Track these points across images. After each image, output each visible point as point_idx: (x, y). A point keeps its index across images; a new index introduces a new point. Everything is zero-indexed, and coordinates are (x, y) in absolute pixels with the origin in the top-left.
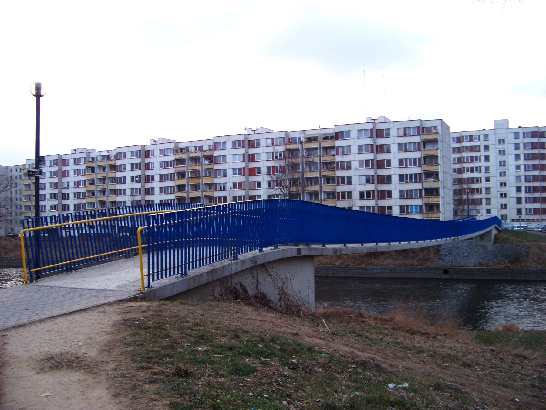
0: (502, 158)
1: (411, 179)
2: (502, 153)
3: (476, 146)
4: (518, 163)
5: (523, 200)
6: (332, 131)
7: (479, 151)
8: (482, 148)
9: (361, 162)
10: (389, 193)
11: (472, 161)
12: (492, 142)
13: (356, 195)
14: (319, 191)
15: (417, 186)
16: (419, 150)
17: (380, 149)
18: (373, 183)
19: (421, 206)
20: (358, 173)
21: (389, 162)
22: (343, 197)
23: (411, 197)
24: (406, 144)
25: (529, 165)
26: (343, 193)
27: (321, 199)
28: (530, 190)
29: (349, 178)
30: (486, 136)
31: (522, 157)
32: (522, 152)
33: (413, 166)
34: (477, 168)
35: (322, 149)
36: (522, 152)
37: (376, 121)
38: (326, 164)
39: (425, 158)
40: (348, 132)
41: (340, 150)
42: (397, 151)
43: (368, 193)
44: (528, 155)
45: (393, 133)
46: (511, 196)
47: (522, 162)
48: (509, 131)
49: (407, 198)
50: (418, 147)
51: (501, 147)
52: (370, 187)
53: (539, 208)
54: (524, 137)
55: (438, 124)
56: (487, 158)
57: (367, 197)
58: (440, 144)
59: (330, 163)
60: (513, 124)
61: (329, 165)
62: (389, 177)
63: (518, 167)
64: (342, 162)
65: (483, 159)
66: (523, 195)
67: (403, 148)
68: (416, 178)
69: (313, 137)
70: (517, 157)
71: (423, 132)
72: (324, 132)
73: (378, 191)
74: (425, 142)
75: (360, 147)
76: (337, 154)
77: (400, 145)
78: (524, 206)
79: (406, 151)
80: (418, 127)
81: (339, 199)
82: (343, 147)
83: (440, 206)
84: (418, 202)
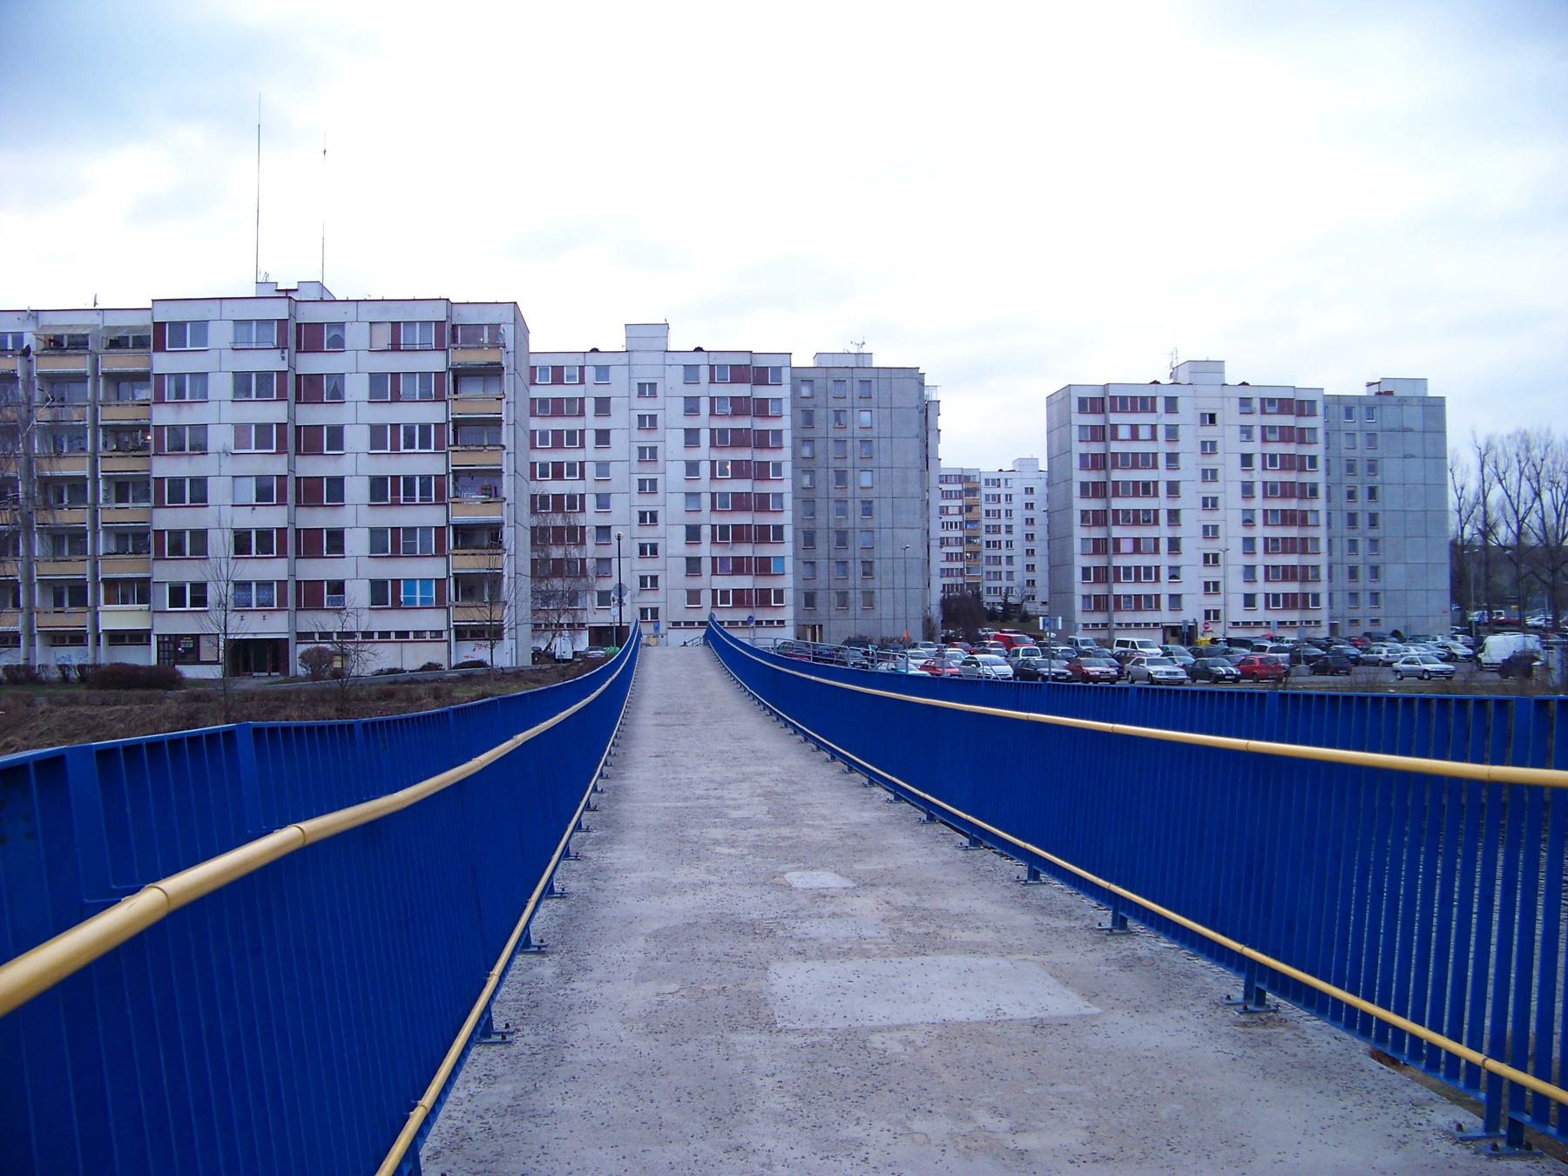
0: (645, 438)
1: (409, 491)
2: (648, 422)
3: (571, 400)
4: (694, 455)
5: (706, 566)
6: (145, 321)
7: (582, 414)
8: (590, 406)
9: (241, 430)
10: (336, 540)
11: (558, 445)
12: (619, 388)
13: (220, 543)
14: (88, 526)
15: (431, 516)
16: (440, 398)
17: (310, 389)
18: (282, 501)
19: (440, 582)
20: (231, 467)
21: (337, 436)
22: (177, 549)
23: (410, 553)
24: (395, 375)
25: (723, 464)
26: (177, 536)
27: (95, 555)
28: (724, 536)
29: (200, 484)
30: (603, 372)
31: (705, 437)
32: (703, 422)
33: (417, 450)
34: (571, 466)
35: (101, 380)
36: (703, 422)
37: (295, 296)
38: (114, 431)
39: (457, 424)
40: (201, 326)
41: (169, 387)
42: (367, 399)
43: (265, 535)
44: (723, 432)
45: (356, 336)
46: (670, 551)
47: (703, 452)
48: (669, 359)
49: (396, 554)
50: (437, 388)
51: (646, 406)
52: (273, 517)
53: (749, 590)
54: (712, 381)
55: (506, 316)
56: (603, 437)
57: (260, 549)
58: (507, 379)
59: (131, 429)
60: (680, 341)
61: (129, 438)
62: (337, 484)
63: (692, 468)
64: (176, 430)
65: (590, 438)
66: (705, 550)
67: (385, 388)
68: (425, 491)
69: (71, 336)
70: (691, 437)
71: (454, 340)
72: (111, 321)
73: (298, 531)
74: (460, 374)
75: (242, 382)
76: (160, 400)
77: (376, 379)
78: (708, 582)
79: (396, 398)
80: (440, 324)
81: (160, 556)
82: (180, 377)
83: (505, 580)
84: (433, 568)
